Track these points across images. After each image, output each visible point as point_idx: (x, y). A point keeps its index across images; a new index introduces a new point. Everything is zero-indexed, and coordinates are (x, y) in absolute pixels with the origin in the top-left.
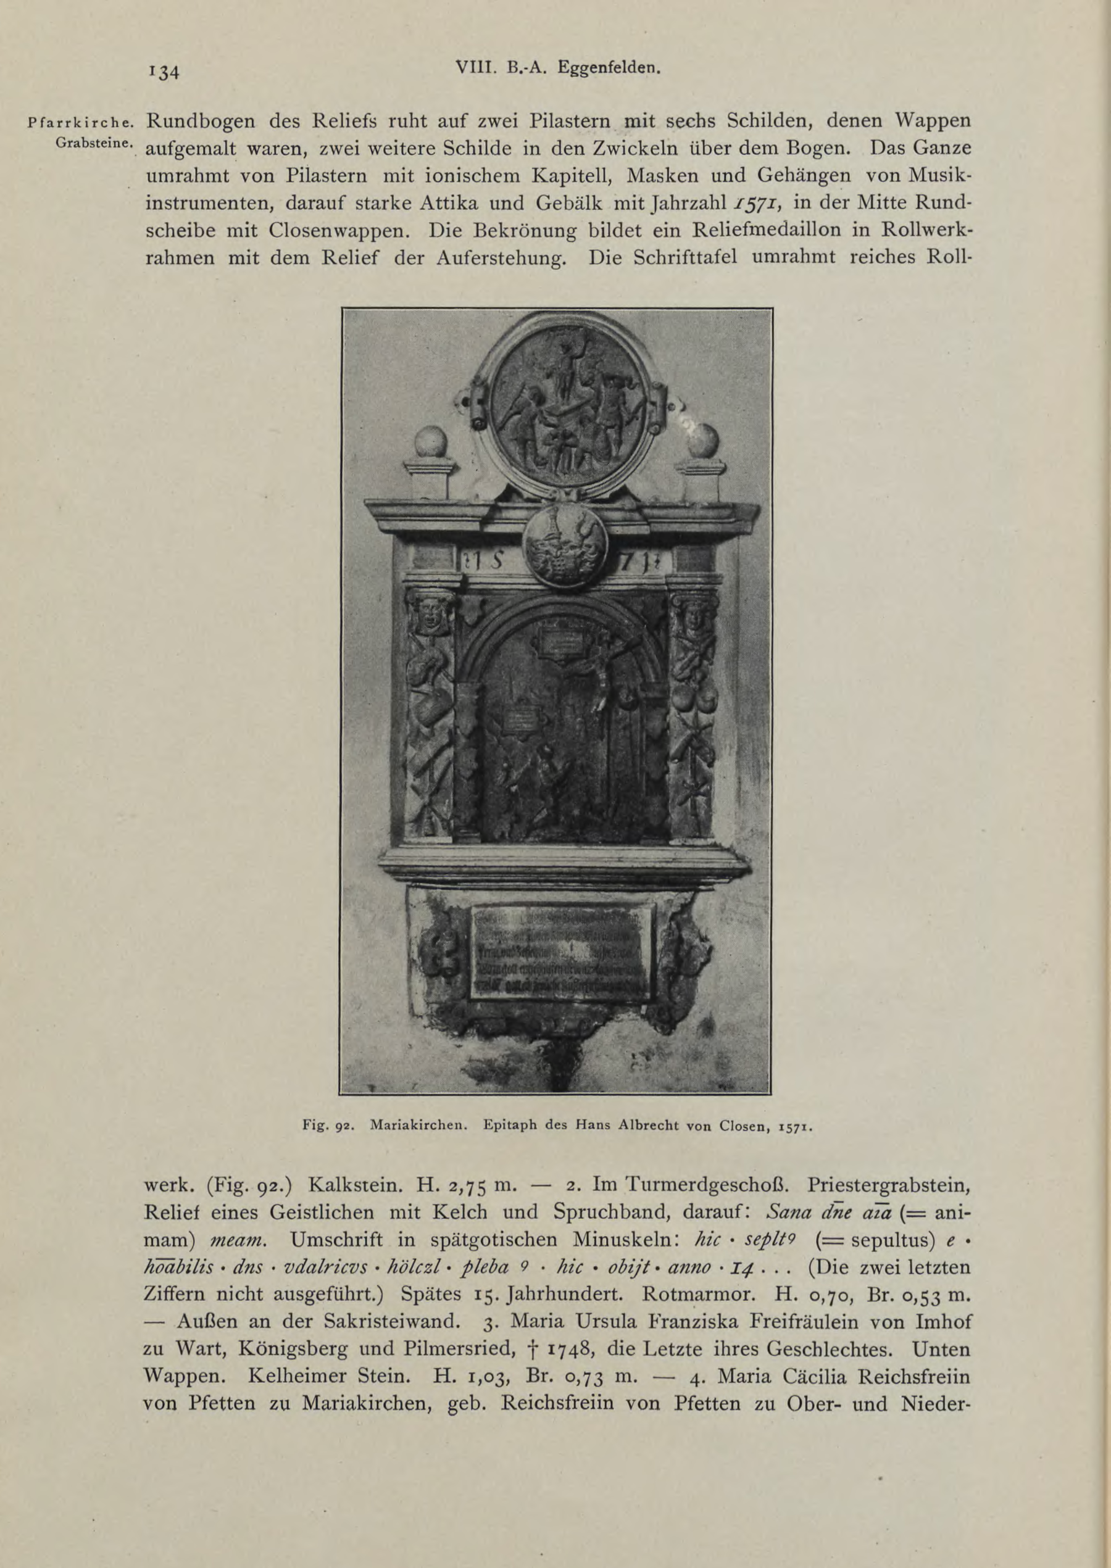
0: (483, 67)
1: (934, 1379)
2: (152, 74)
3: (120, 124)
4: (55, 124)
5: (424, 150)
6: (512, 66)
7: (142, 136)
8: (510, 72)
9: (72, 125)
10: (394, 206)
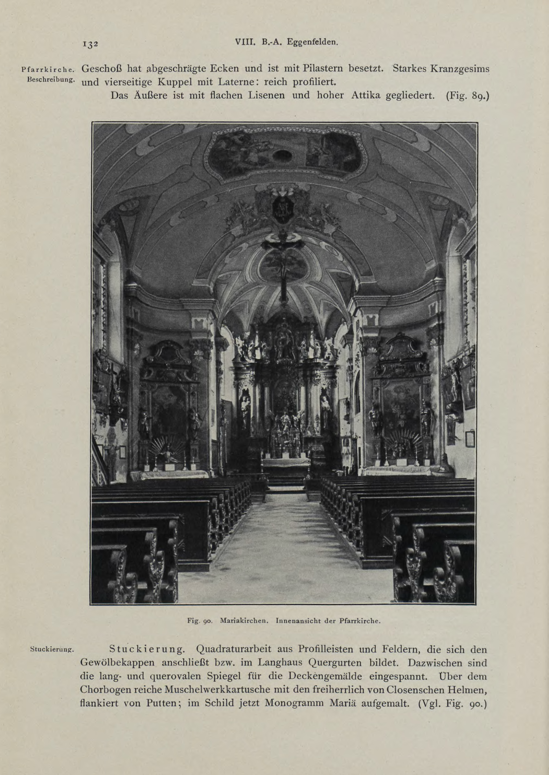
0: (249, 42)
1: (320, 690)
2: (85, 45)
3: (68, 70)
4: (35, 70)
5: (162, 96)
6: (265, 41)
7: (80, 76)
8: (264, 44)
9: (44, 70)
10: (414, 70)
